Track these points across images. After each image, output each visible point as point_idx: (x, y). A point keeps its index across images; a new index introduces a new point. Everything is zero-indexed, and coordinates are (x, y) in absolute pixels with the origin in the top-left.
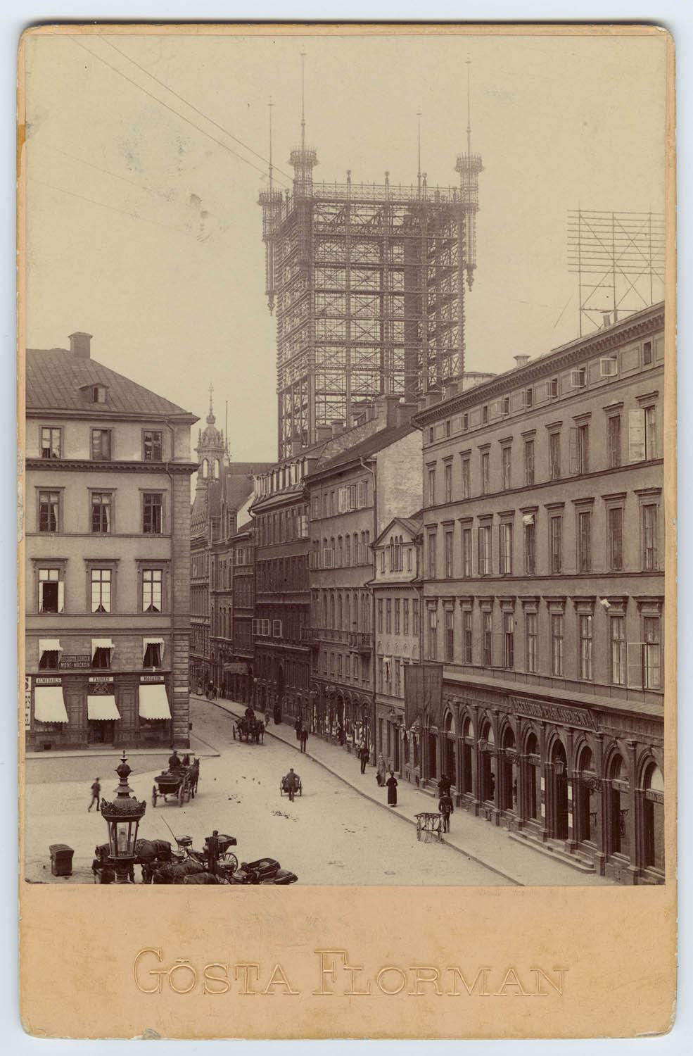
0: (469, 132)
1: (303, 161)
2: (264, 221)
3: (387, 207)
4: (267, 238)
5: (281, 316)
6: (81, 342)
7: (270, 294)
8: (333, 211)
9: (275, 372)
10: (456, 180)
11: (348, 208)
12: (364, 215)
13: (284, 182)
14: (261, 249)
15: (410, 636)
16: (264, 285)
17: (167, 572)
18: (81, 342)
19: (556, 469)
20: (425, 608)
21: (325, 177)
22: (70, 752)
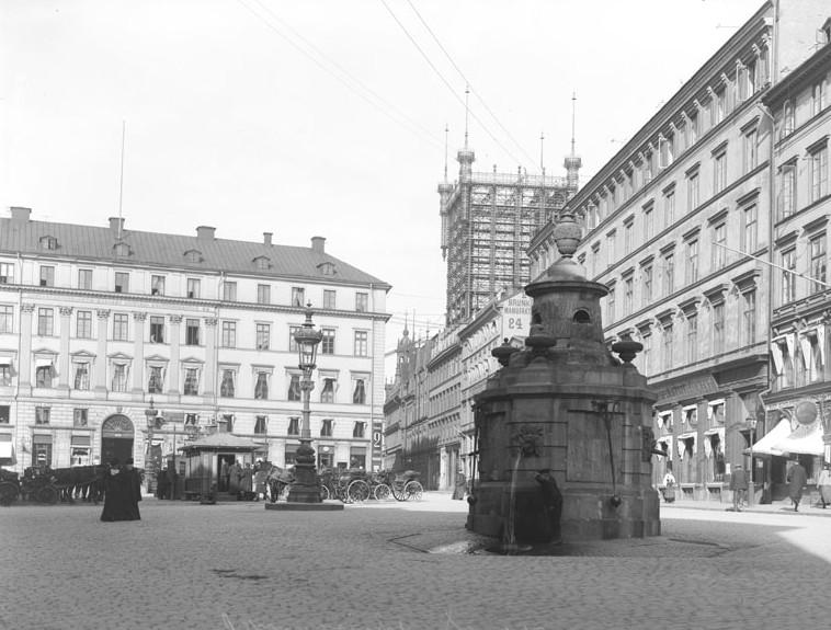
0: (573, 142)
1: (466, 159)
2: (441, 202)
3: (519, 188)
4: (442, 214)
5: (450, 262)
6: (319, 241)
7: (444, 248)
8: (484, 191)
9: (446, 295)
10: (564, 172)
11: (495, 190)
12: (502, 197)
13: (453, 177)
14: (439, 219)
15: (767, 23)
16: (440, 241)
17: (157, 333)
18: (319, 241)
19: (753, 341)
20: (32, 363)
21: (481, 171)
22: (689, 521)
